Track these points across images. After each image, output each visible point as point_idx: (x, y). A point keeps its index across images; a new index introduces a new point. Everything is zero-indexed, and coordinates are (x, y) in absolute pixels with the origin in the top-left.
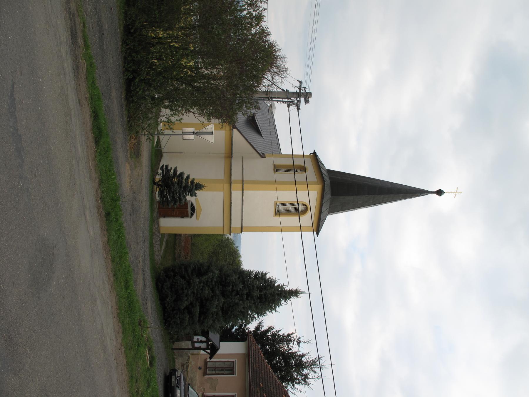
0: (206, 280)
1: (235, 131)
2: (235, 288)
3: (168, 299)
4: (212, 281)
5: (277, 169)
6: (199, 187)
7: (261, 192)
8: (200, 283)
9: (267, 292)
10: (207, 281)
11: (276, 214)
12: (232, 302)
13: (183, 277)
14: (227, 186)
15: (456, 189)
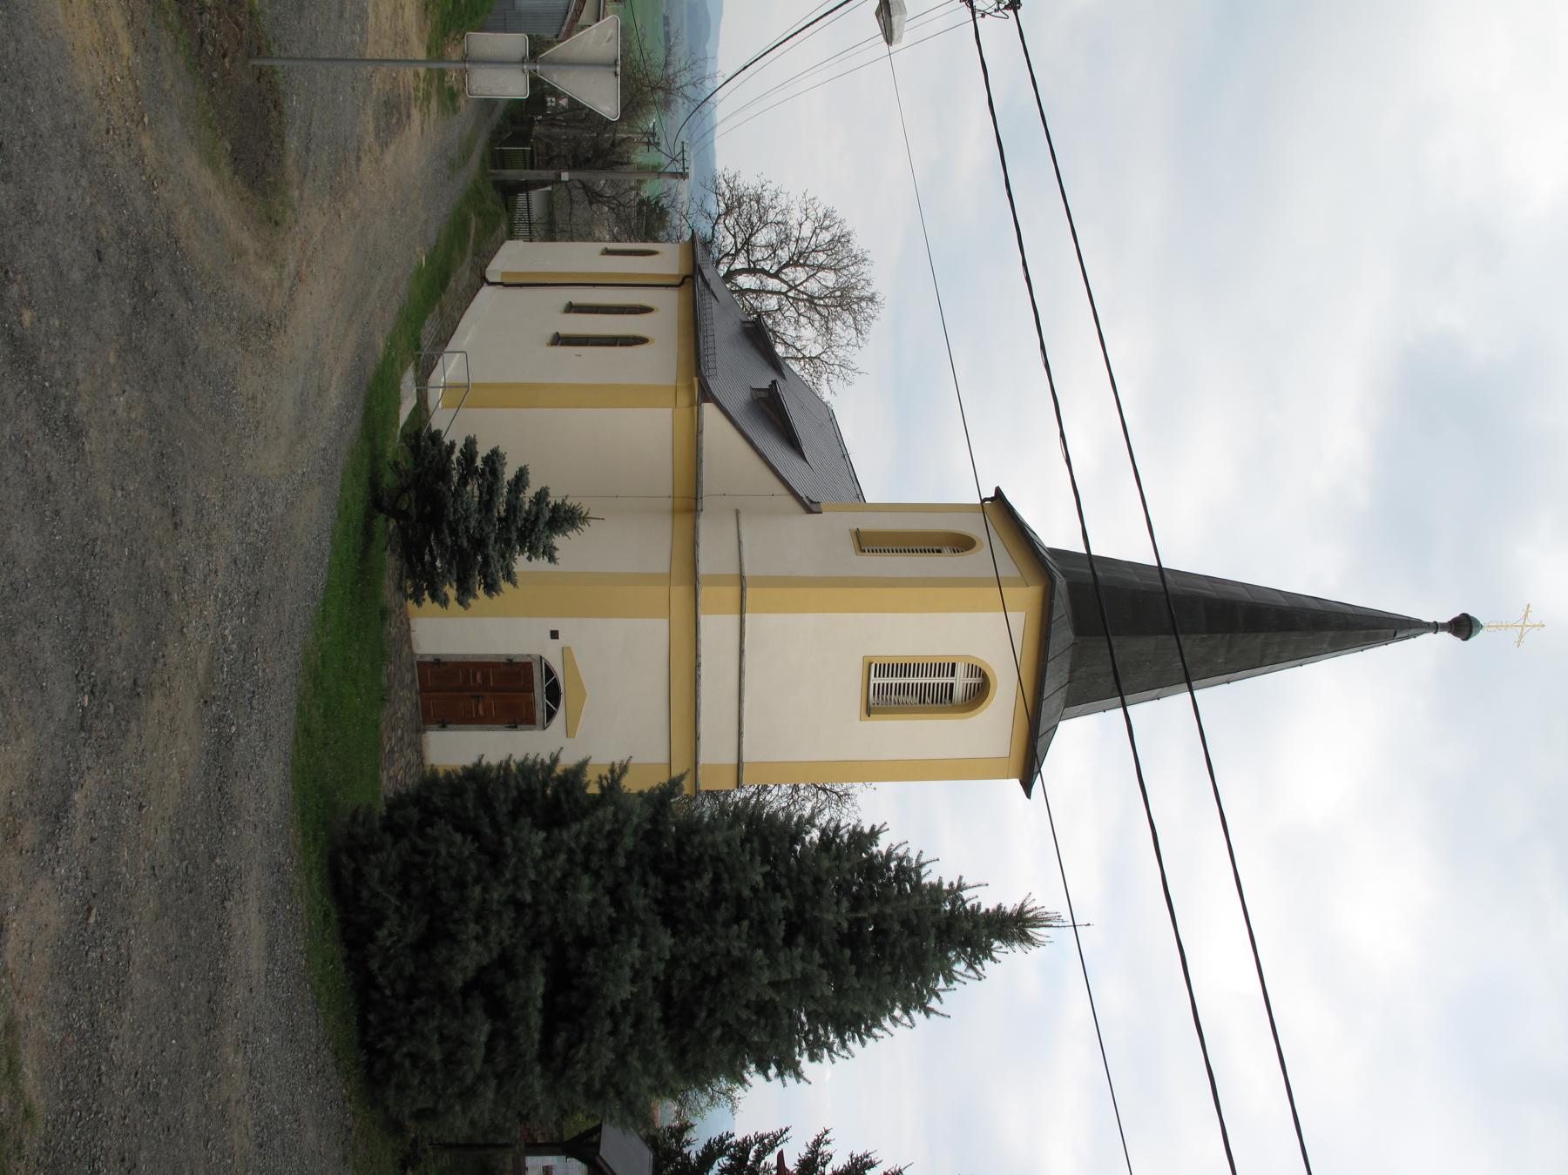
0: (584, 839)
1: (709, 409)
2: (727, 886)
3: (385, 932)
4: (611, 851)
5: (865, 542)
6: (565, 518)
7: (809, 620)
8: (550, 855)
9: (888, 910)
10: (588, 850)
11: (869, 711)
12: (713, 954)
13: (468, 828)
14: (680, 593)
15: (1524, 613)
